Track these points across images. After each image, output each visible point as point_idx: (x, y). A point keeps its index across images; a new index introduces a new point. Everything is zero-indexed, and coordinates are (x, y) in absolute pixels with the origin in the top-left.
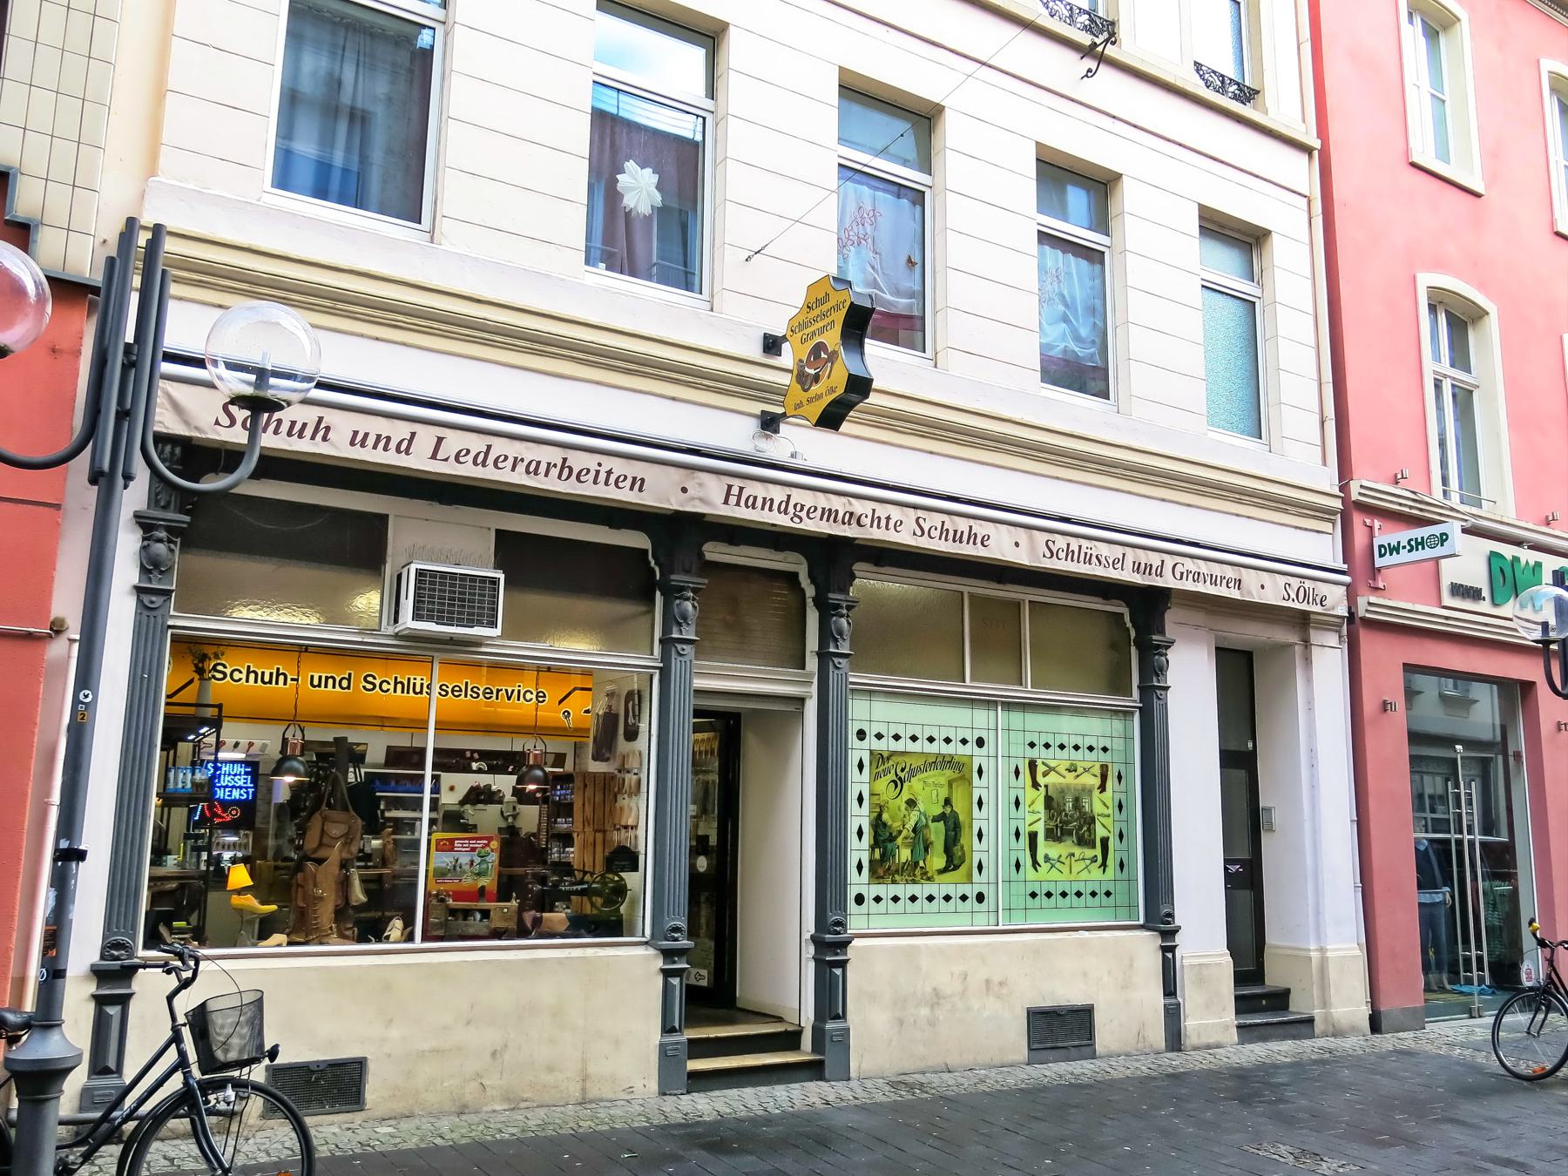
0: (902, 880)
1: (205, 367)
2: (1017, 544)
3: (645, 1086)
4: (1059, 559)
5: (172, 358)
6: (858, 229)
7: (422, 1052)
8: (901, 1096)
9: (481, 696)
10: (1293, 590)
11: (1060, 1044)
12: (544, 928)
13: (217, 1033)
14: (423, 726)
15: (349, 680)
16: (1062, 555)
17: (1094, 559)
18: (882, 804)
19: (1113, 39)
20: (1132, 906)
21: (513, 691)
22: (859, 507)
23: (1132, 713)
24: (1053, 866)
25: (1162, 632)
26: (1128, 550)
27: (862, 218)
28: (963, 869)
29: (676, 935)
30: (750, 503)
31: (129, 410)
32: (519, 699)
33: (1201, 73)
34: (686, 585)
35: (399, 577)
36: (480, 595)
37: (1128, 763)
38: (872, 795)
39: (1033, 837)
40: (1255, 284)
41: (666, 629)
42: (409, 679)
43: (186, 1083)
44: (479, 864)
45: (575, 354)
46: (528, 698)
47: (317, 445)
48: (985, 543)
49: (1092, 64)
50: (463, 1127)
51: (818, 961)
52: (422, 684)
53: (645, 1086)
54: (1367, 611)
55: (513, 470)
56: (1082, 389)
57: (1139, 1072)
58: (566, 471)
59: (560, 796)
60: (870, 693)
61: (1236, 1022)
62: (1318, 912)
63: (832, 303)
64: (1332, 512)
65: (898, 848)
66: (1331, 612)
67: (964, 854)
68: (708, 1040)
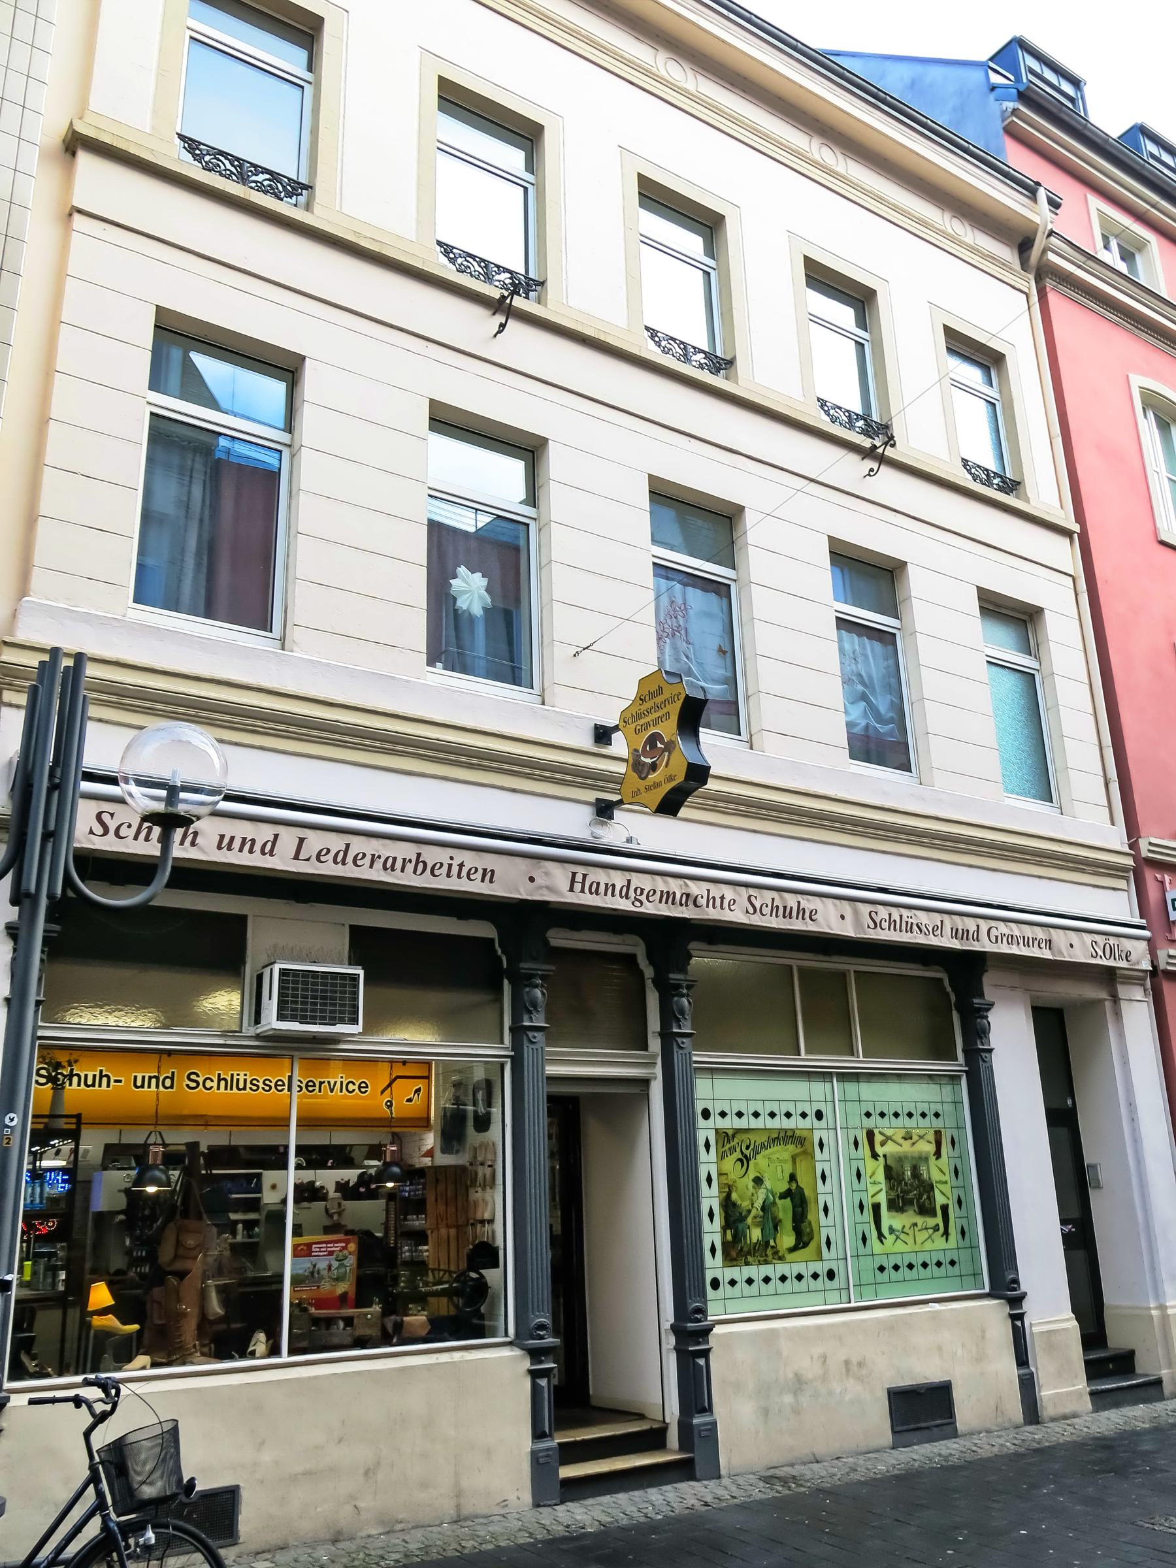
0: (754, 1261)
1: (118, 785)
2: (843, 917)
3: (519, 1498)
4: (883, 929)
5: (90, 777)
6: (672, 622)
7: (295, 1475)
8: (778, 1492)
9: (273, 1089)
10: (1099, 948)
11: (923, 1425)
12: (405, 1334)
13: (135, 1471)
14: (284, 1123)
15: (172, 1079)
16: (885, 925)
17: (915, 927)
18: (730, 1183)
19: (892, 442)
20: (976, 1274)
21: (335, 1083)
22: (695, 888)
23: (959, 1077)
24: (898, 1237)
25: (982, 995)
26: (946, 917)
27: (675, 611)
28: (813, 1245)
29: (541, 1333)
30: (593, 890)
31: (53, 831)
32: (341, 1091)
33: (968, 468)
34: (534, 972)
35: (260, 978)
36: (341, 992)
37: (960, 1128)
38: (720, 1174)
39: (876, 1208)
40: (1033, 658)
41: (516, 1018)
42: (232, 1075)
43: (105, 1527)
44: (337, 1268)
45: (421, 752)
46: (351, 1090)
47: (185, 850)
48: (814, 917)
49: (875, 466)
50: (342, 1556)
51: (680, 1351)
52: (245, 1080)
53: (519, 1498)
54: (1168, 963)
55: (371, 866)
56: (881, 761)
57: (1006, 1449)
58: (421, 866)
59: (409, 1192)
60: (713, 1071)
61: (1088, 1389)
62: (1153, 1269)
63: (666, 694)
64: (1124, 869)
65: (749, 1227)
66: (1137, 967)
67: (812, 1230)
68: (575, 1443)
